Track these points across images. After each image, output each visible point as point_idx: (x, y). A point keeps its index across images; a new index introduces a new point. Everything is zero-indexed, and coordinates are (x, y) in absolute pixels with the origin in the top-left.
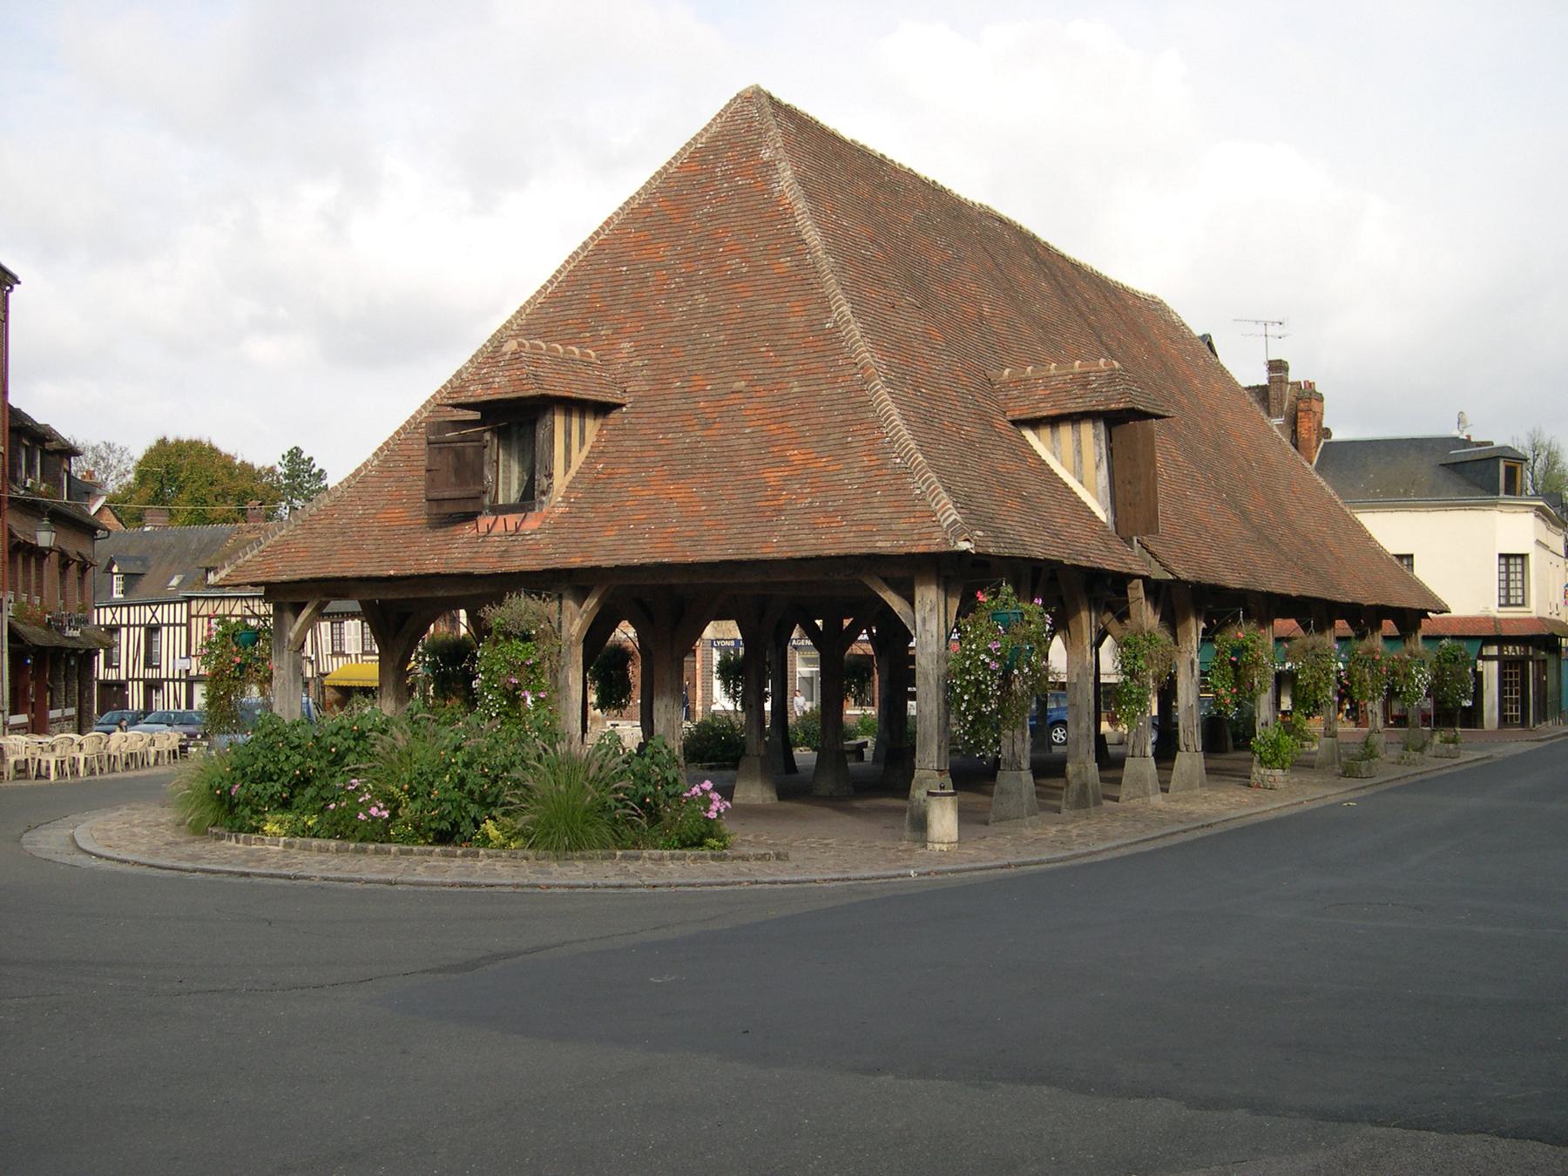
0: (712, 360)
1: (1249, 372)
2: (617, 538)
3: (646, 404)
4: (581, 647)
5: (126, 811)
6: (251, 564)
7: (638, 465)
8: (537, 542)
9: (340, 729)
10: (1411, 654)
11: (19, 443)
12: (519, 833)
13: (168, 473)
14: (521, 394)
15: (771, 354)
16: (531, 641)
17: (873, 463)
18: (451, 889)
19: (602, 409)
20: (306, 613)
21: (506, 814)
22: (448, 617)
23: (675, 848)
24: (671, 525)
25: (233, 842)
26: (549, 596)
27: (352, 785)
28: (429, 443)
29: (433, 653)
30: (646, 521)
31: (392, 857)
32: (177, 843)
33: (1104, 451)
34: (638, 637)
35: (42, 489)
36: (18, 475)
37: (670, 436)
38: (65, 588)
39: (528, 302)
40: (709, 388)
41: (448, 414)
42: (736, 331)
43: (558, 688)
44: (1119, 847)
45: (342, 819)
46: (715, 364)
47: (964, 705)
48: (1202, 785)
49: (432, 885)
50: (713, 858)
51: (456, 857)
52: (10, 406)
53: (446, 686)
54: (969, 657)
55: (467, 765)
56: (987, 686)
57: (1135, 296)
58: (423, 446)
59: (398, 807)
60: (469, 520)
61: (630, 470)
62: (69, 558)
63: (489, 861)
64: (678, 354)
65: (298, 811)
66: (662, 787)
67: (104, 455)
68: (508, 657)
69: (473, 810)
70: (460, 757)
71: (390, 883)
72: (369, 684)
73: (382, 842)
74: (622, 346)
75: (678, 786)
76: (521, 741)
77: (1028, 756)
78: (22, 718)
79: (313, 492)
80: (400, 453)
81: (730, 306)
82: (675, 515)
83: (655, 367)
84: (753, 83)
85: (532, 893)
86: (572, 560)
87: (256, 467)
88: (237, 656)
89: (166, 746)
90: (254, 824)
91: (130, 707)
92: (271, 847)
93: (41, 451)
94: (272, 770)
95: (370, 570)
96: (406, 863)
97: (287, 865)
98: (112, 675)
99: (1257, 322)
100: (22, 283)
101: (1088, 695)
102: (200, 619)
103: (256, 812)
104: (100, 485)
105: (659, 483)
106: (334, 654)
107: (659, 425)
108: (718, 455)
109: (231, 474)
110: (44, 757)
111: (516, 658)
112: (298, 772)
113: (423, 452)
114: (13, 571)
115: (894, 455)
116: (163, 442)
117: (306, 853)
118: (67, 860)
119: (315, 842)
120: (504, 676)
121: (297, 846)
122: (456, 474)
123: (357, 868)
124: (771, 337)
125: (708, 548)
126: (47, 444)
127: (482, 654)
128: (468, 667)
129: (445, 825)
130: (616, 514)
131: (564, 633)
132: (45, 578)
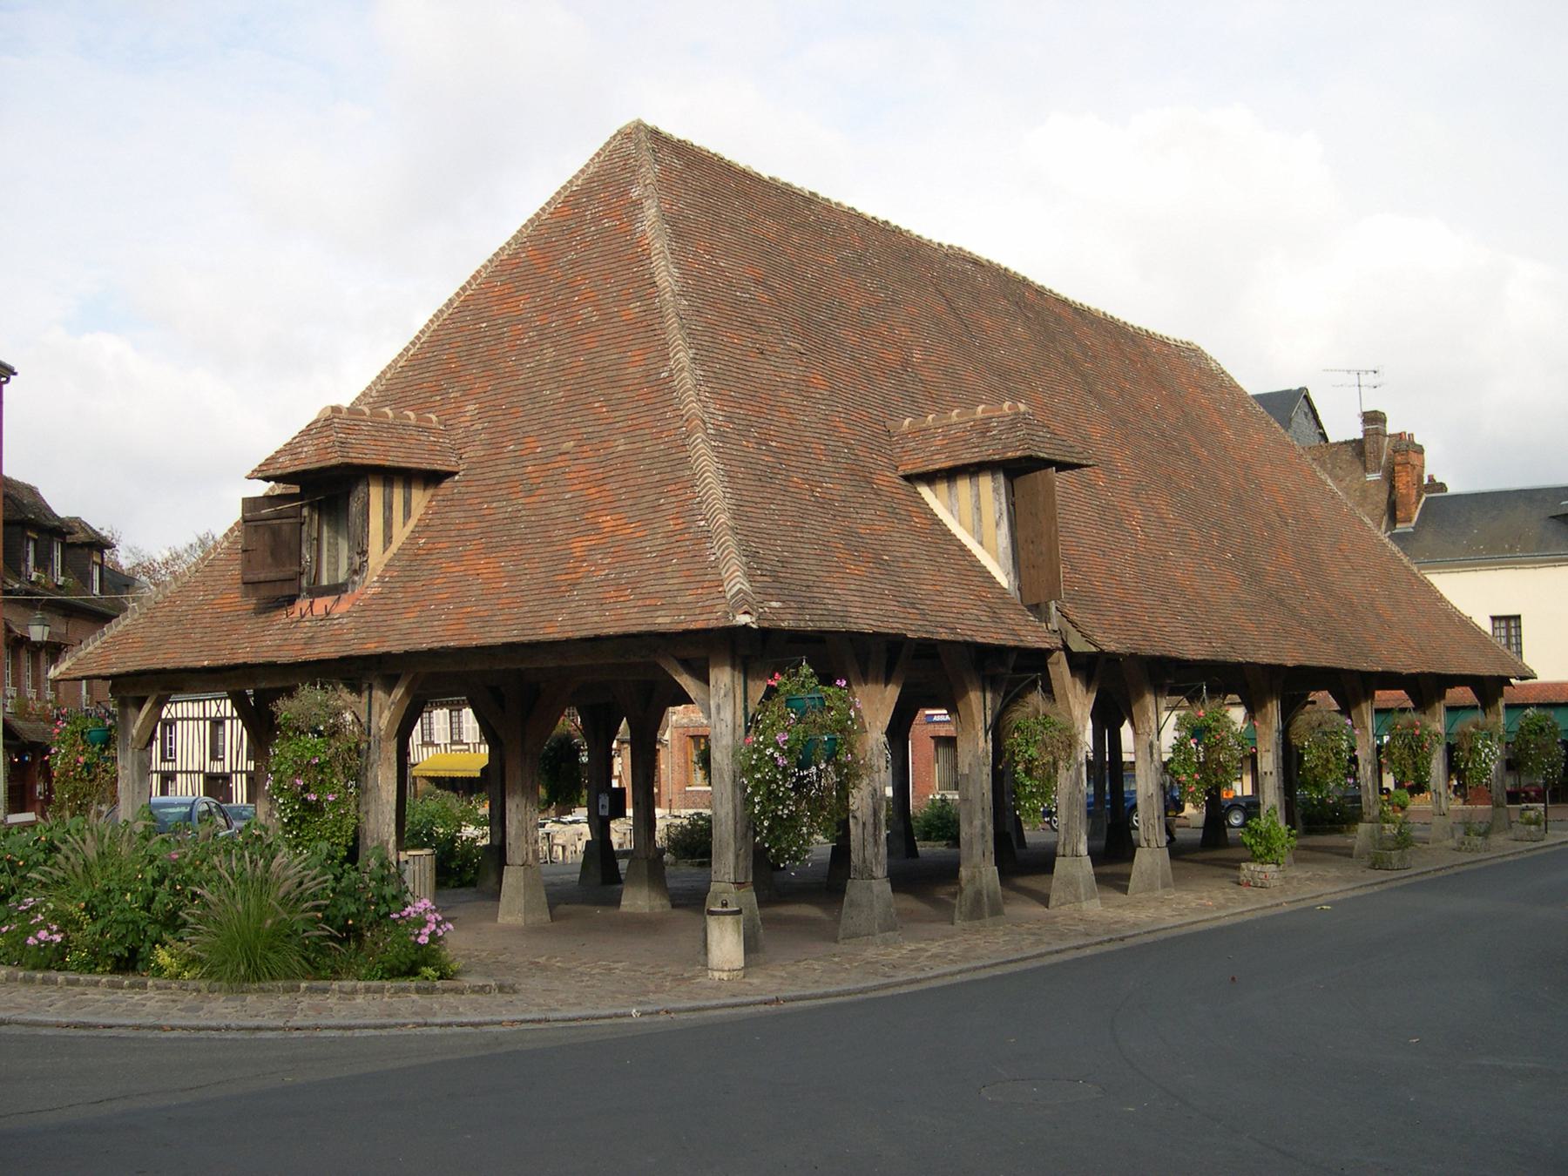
1: (1342, 426)
10: (1476, 726)
14: (323, 464)
15: (604, 410)
17: (678, 527)
19: (432, 478)
33: (1004, 506)
37: (494, 505)
39: (389, 367)
40: (539, 450)
42: (576, 386)
44: (960, 972)
46: (548, 425)
47: (758, 808)
48: (1165, 885)
50: (418, 990)
54: (755, 750)
56: (779, 786)
57: (1163, 342)
64: (517, 415)
77: (885, 861)
81: (574, 359)
84: (634, 118)
93: (62, 544)
99: (1349, 371)
100: (19, 374)
101: (982, 788)
106: (424, 744)
107: (486, 494)
108: (534, 524)
115: (700, 517)
122: (272, 554)
124: (606, 391)
126: (68, 537)
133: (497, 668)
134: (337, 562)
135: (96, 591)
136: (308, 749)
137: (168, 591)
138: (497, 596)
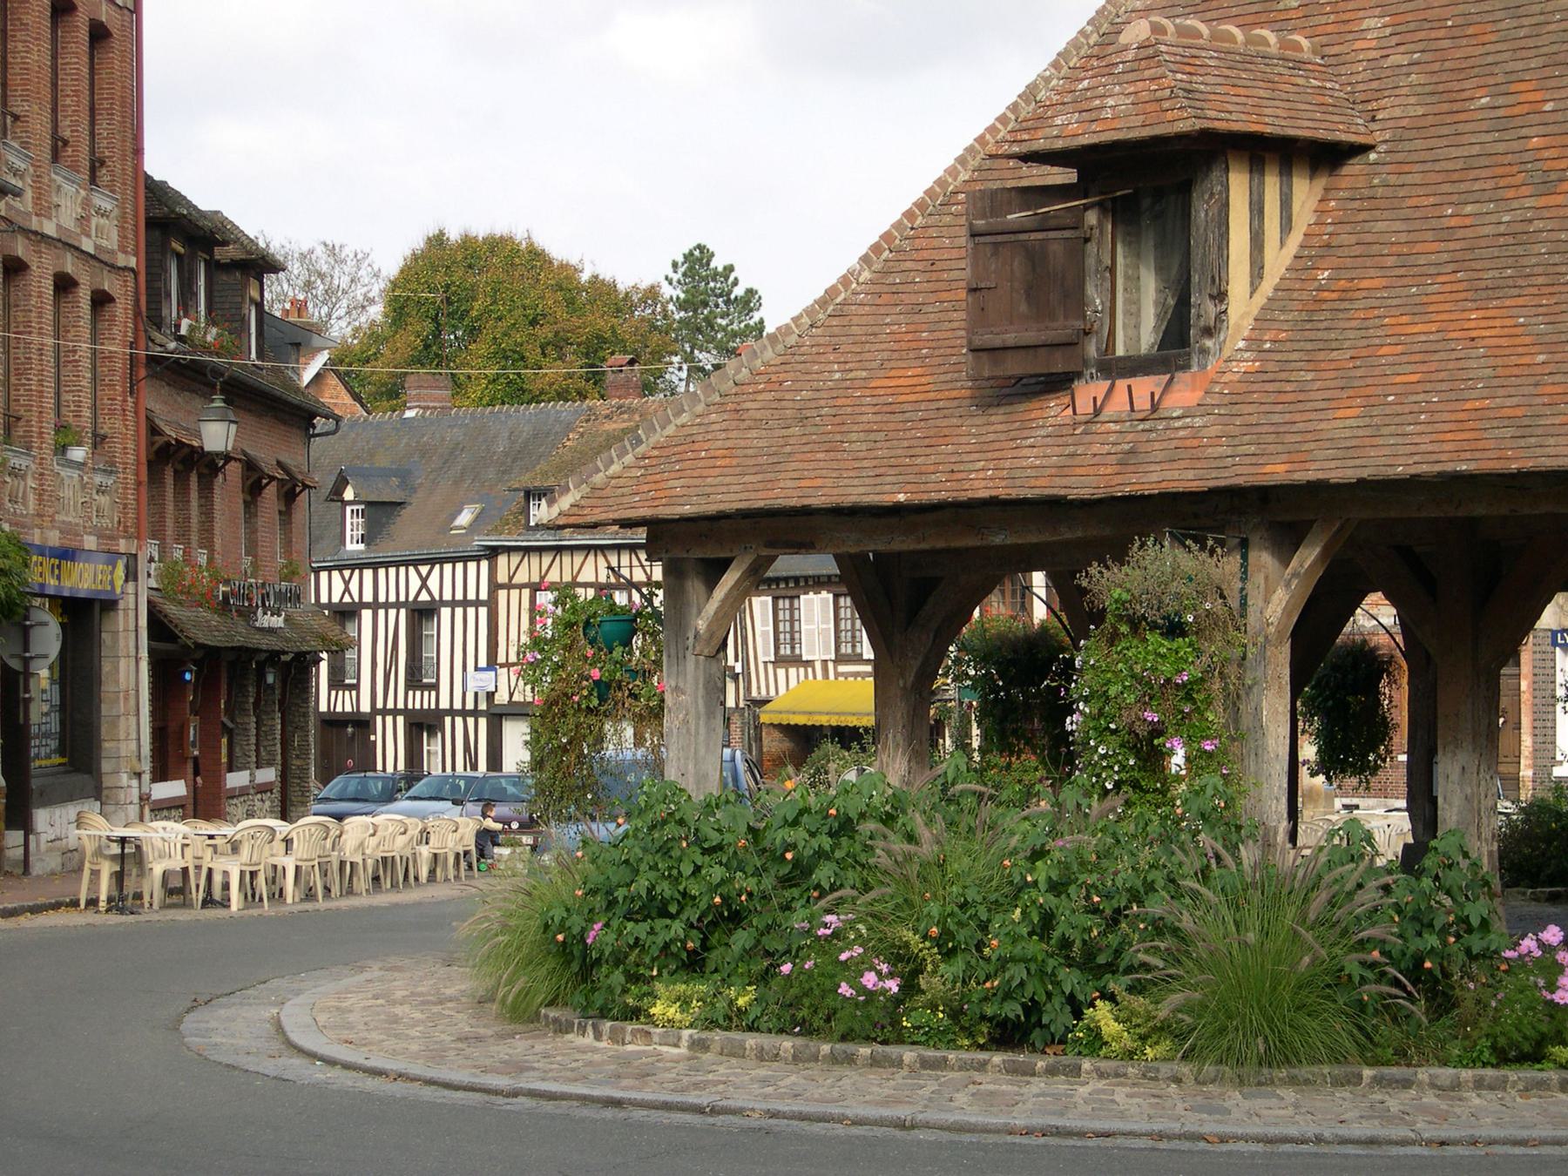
0: (1555, 48)
2: (1361, 422)
3: (1419, 144)
4: (1286, 649)
5: (377, 973)
6: (622, 482)
7: (1402, 271)
8: (1196, 433)
9: (802, 812)
11: (165, 248)
12: (1163, 1029)
13: (449, 302)
16: (1183, 634)
18: (1025, 1140)
20: (729, 579)
21: (1135, 989)
22: (1008, 586)
23: (1484, 1065)
24: (1475, 394)
25: (589, 1039)
26: (1222, 543)
27: (826, 926)
28: (974, 235)
29: (983, 659)
30: (1420, 388)
31: (905, 1072)
32: (479, 1039)
34: (1403, 624)
35: (209, 338)
36: (165, 312)
37: (1469, 209)
38: (255, 531)
40: (1549, 107)
41: (1008, 174)
43: (1241, 733)
45: (806, 995)
49: (986, 1130)
51: (1033, 1075)
52: (148, 178)
53: (1010, 726)
55: (1057, 888)
58: (963, 241)
59: (919, 971)
60: (1058, 390)
61: (1384, 282)
62: (263, 475)
63: (1101, 1084)
65: (717, 977)
66: (1458, 937)
67: (325, 268)
68: (1138, 669)
69: (1070, 979)
70: (1043, 872)
71: (901, 1125)
72: (852, 722)
73: (885, 1042)
74: (1366, 24)
75: (1492, 936)
76: (1166, 839)
78: (175, 789)
79: (735, 335)
80: (915, 256)
82: (1480, 373)
83: (1436, 66)
85: (1190, 1151)
86: (1268, 469)
87: (621, 287)
88: (593, 665)
89: (451, 844)
90: (630, 1001)
91: (379, 766)
92: (665, 1049)
94: (667, 894)
95: (858, 492)
96: (932, 1086)
97: (696, 1086)
98: (344, 703)
102: (515, 593)
103: (634, 978)
104: (317, 329)
105: (1447, 307)
106: (780, 661)
107: (1446, 188)
109: (571, 302)
110: (219, 865)
111: (1154, 669)
112: (718, 900)
113: (963, 253)
114: (156, 499)
116: (437, 241)
117: (734, 1061)
118: (270, 1067)
119: (752, 1040)
120: (1129, 707)
121: (716, 1047)
123: (835, 1093)
125: (1552, 441)
126: (217, 250)
127: (1085, 662)
128: (1058, 688)
129: (1013, 1010)
130: (1359, 373)
131: (1252, 619)
132: (217, 515)
133: (1526, 511)
134: (1138, 314)
135: (253, 355)
136: (1163, 656)
137: (758, 362)
138: (1532, 380)
